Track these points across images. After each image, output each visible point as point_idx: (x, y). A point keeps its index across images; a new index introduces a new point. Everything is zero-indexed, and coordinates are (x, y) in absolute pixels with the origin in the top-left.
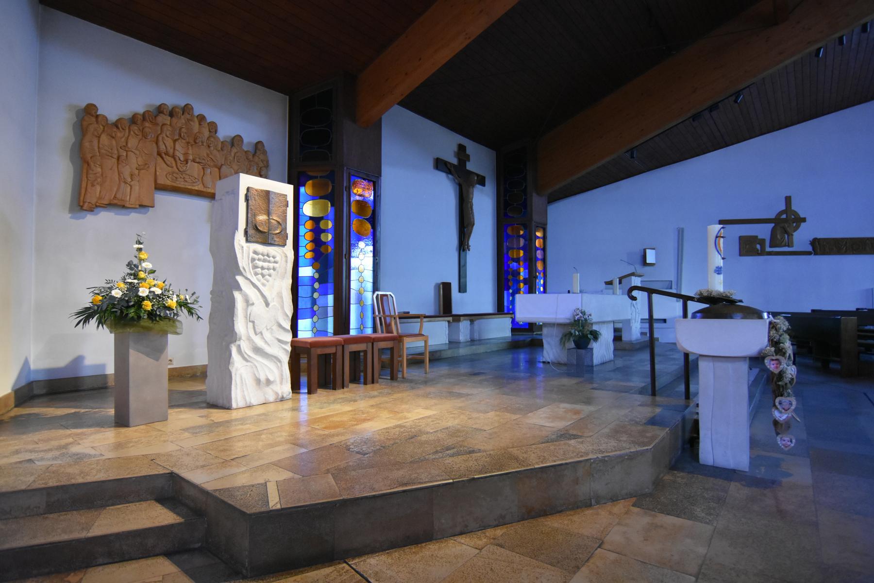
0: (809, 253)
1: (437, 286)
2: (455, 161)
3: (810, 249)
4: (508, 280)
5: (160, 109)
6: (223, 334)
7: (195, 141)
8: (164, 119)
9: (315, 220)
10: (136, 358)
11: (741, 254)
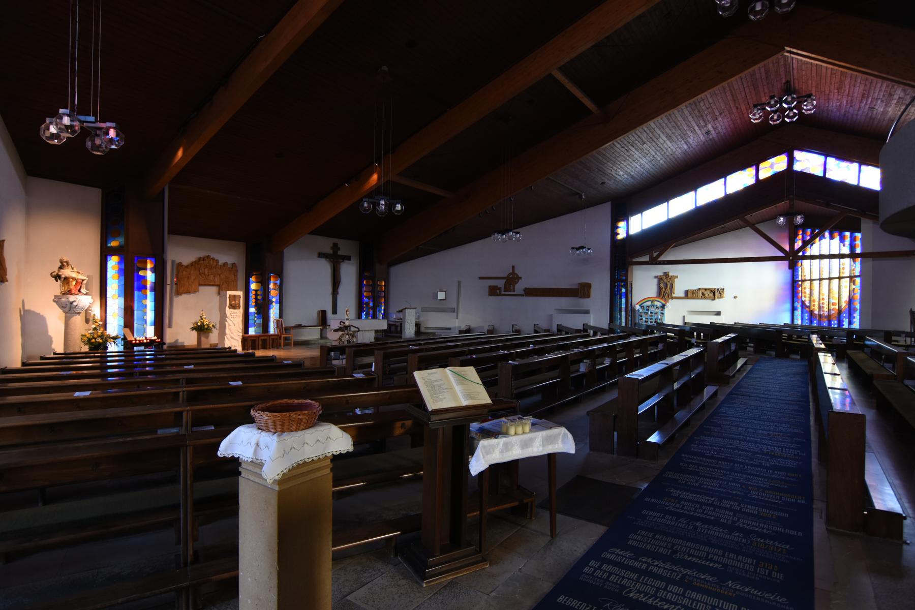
1: (319, 312)
2: (331, 252)
5: (200, 259)
9: (256, 291)
10: (203, 339)
11: (490, 295)
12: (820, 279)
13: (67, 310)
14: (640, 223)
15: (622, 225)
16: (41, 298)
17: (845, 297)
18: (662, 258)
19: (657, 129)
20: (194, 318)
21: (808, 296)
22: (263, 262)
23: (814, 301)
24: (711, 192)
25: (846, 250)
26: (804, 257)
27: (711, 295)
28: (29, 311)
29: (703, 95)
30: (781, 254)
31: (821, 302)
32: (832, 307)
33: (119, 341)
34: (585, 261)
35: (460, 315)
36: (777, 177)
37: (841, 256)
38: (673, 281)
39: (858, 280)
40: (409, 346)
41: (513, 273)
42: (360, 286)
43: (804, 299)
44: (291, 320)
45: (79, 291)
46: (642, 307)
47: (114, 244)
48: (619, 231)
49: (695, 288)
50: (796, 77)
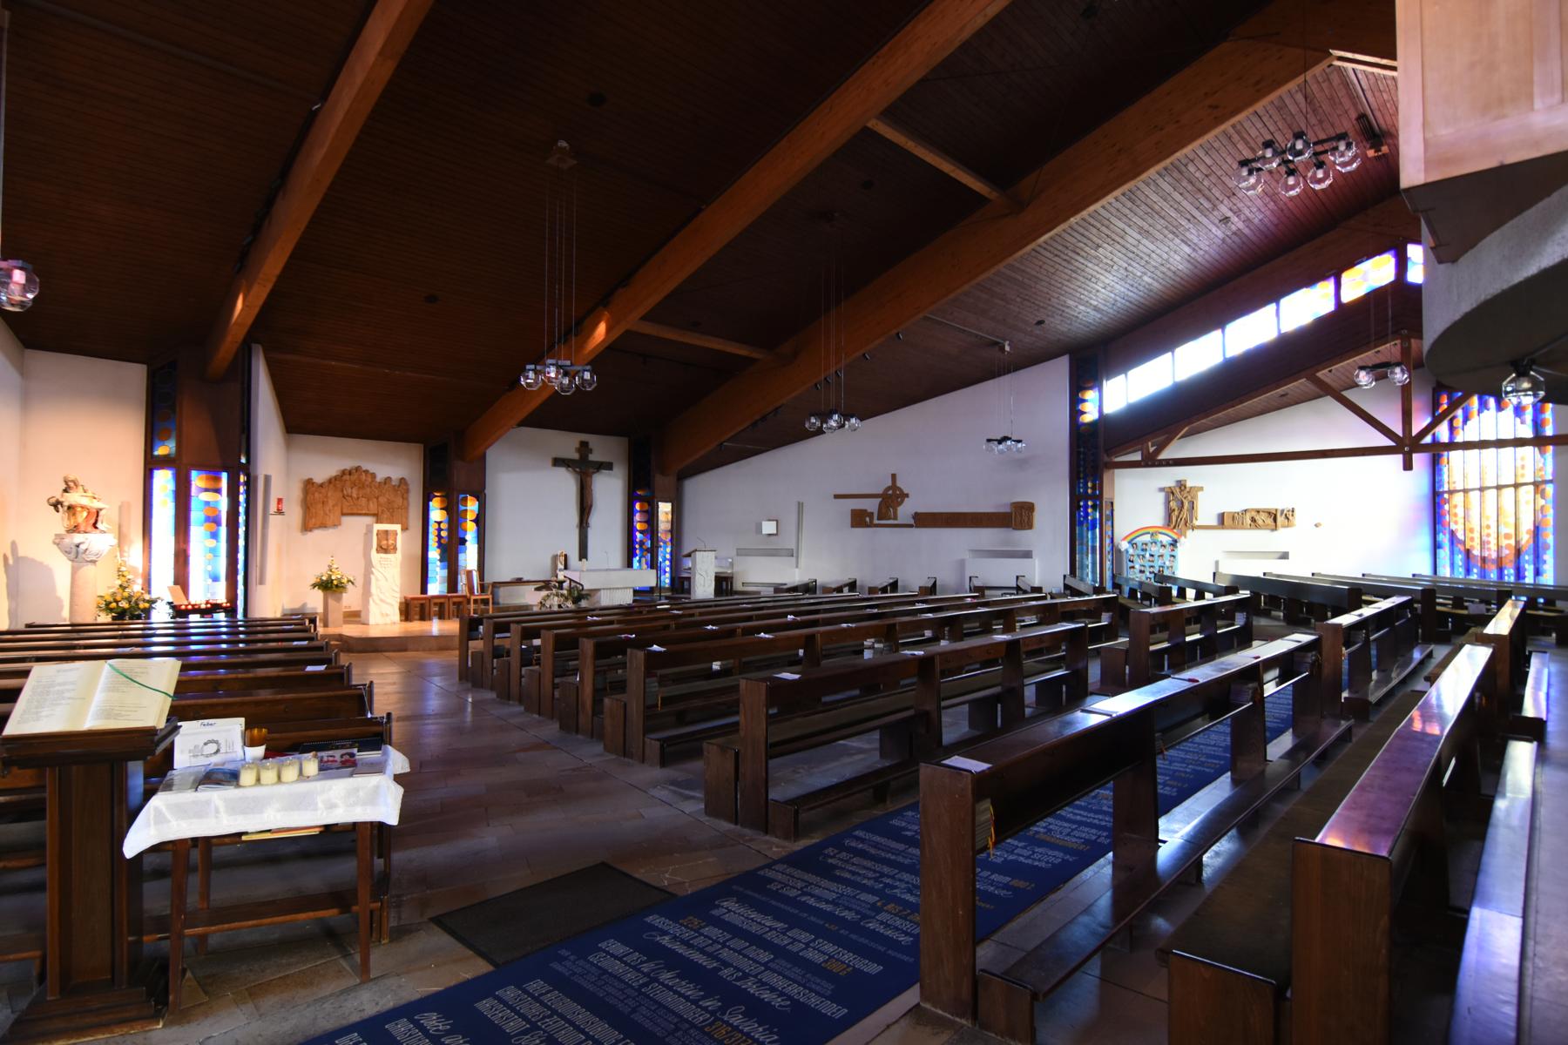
2: (576, 456)
5: (344, 472)
7: (362, 486)
10: (331, 602)
12: (1482, 489)
13: (72, 556)
14: (1124, 391)
15: (1091, 395)
16: (40, 537)
17: (1527, 525)
18: (1163, 456)
19: (1113, 219)
20: (319, 571)
21: (1461, 521)
22: (452, 471)
23: (1472, 531)
24: (1254, 330)
25: (1527, 432)
26: (1452, 446)
27: (1270, 521)
28: (25, 559)
29: (1187, 150)
30: (1390, 443)
31: (1485, 532)
32: (1504, 542)
34: (1022, 463)
36: (1376, 297)
37: (1519, 442)
38: (1195, 497)
39: (1550, 489)
41: (894, 486)
42: (630, 513)
43: (1453, 527)
44: (501, 570)
45: (95, 526)
46: (1133, 544)
47: (161, 451)
48: (1086, 407)
49: (1238, 509)
50: (1374, 106)
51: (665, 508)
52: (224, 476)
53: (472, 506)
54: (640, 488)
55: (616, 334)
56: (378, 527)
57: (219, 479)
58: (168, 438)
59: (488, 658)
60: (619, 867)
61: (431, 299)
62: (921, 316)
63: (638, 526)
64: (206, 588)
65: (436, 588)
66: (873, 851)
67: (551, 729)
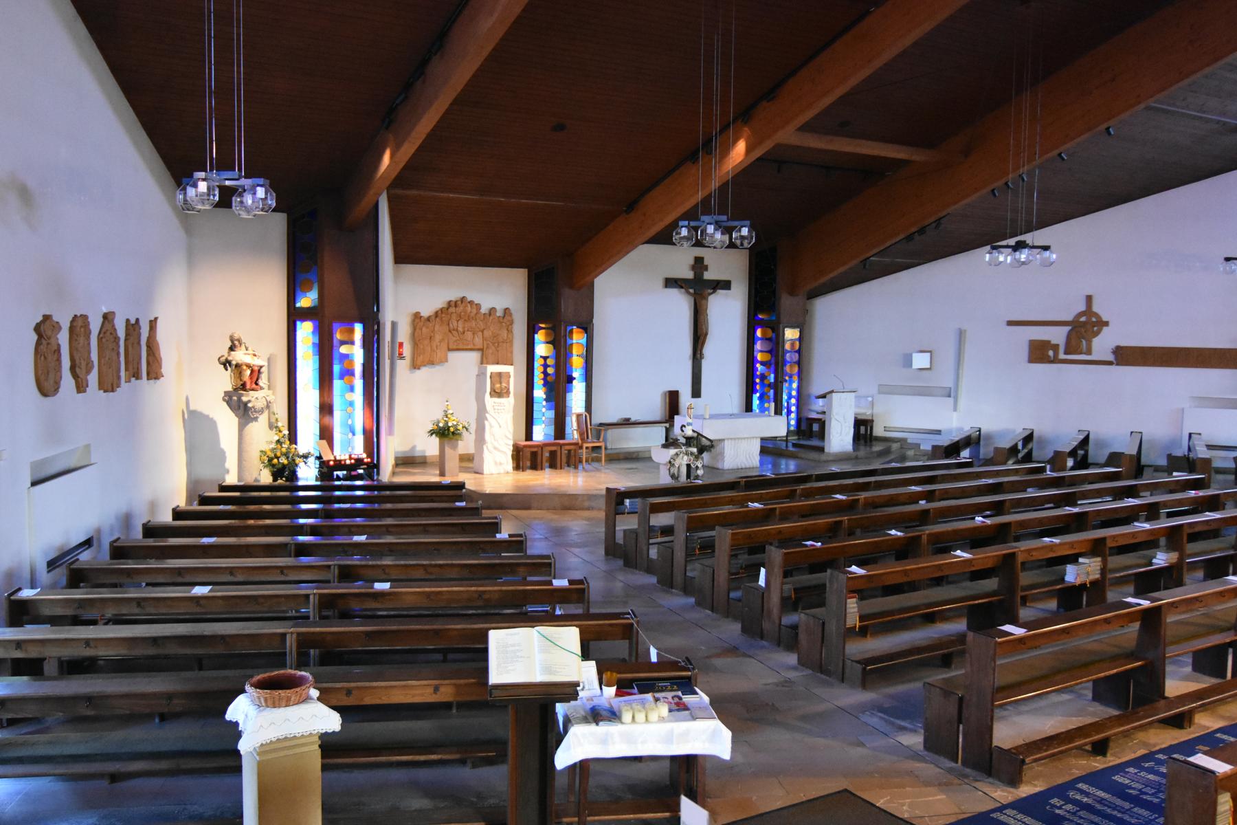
0: (1110, 363)
2: (690, 275)
3: (1111, 358)
4: (755, 384)
6: (480, 440)
7: (469, 318)
8: (452, 309)
9: (545, 358)
10: (448, 450)
11: (1031, 360)
20: (432, 415)
33: (311, 460)
35: (962, 402)
40: (743, 502)
41: (1089, 311)
42: (751, 340)
44: (606, 412)
51: (791, 334)
52: (358, 328)
53: (578, 339)
54: (762, 311)
55: (758, 153)
56: (492, 369)
57: (352, 331)
58: (310, 289)
59: (642, 539)
60: (858, 794)
61: (560, 128)
62: (1142, 106)
63: (759, 357)
64: (349, 447)
65: (541, 433)
66: (1098, 806)
67: (732, 630)
